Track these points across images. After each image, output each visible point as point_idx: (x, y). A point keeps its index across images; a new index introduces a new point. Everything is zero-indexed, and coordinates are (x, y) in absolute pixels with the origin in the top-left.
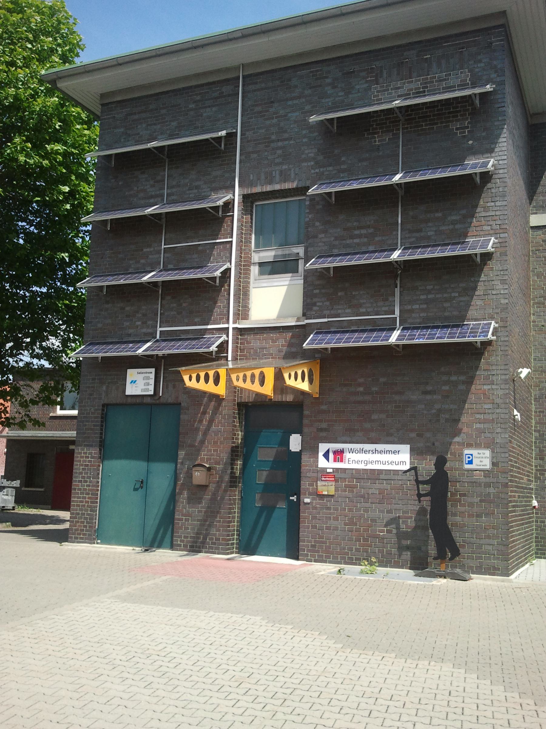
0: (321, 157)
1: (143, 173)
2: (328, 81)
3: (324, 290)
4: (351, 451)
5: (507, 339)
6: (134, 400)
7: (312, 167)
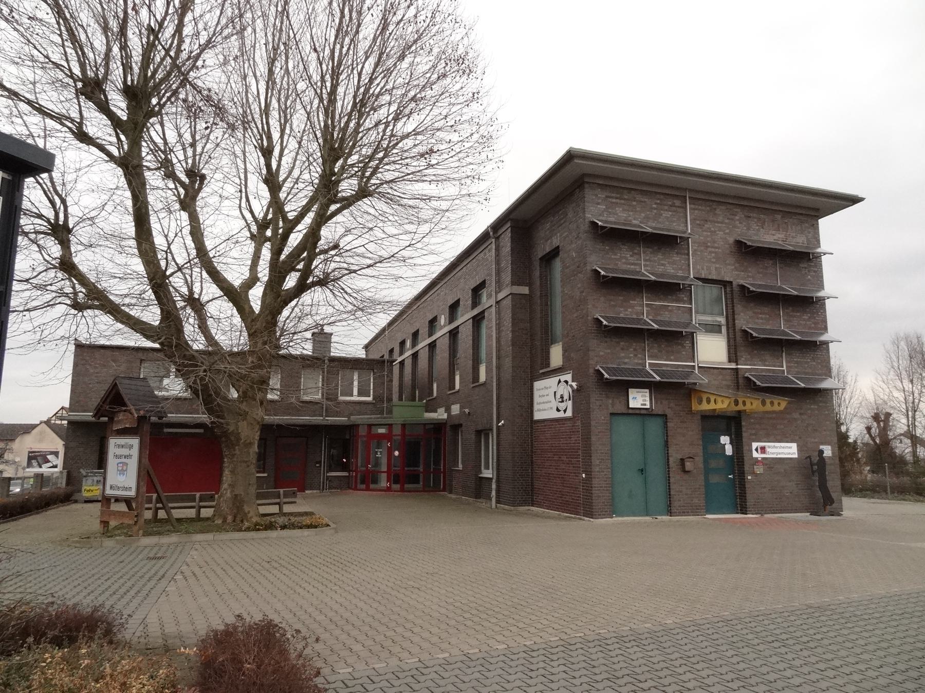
0: (737, 265)
4: (769, 447)
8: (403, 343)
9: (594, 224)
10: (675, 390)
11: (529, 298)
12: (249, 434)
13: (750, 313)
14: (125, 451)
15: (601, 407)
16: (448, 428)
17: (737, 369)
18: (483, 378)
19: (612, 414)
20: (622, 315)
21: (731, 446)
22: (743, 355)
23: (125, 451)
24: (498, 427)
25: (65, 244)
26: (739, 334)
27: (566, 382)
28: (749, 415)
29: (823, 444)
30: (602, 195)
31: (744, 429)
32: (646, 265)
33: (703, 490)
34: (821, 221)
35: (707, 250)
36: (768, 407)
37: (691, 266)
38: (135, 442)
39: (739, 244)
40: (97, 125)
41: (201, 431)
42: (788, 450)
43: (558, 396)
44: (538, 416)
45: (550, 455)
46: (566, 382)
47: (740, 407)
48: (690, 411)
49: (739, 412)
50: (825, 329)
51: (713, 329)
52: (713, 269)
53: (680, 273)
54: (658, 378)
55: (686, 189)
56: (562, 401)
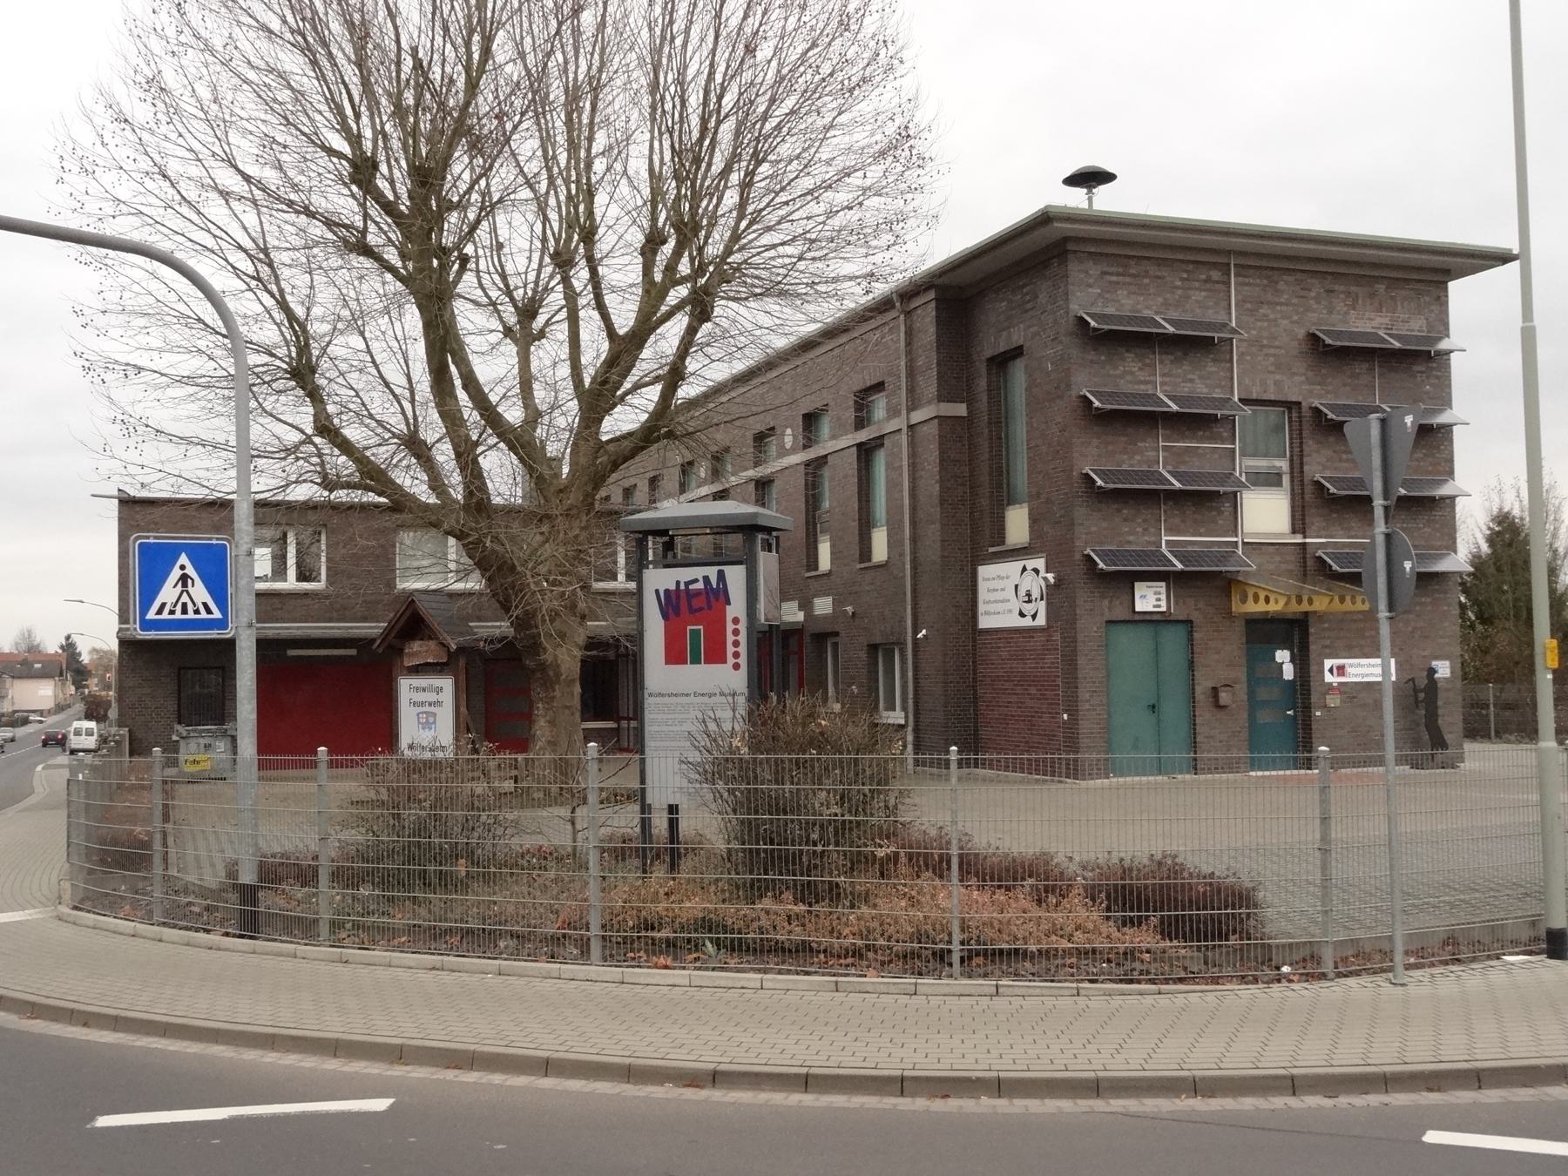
0: (1310, 374)
2: (1313, 294)
9: (1082, 322)
10: (1205, 582)
11: (968, 422)
14: (432, 697)
15: (1092, 611)
16: (807, 639)
17: (1304, 544)
18: (880, 551)
19: (1109, 622)
20: (1124, 467)
22: (1315, 522)
23: (432, 697)
24: (916, 641)
25: (315, 395)
26: (1309, 489)
27: (1036, 571)
28: (1321, 617)
29: (1437, 658)
30: (1095, 270)
31: (1311, 639)
32: (1163, 385)
33: (1245, 735)
35: (1263, 352)
36: (1348, 606)
37: (1233, 382)
38: (446, 684)
39: (1313, 338)
41: (353, 652)
43: (1022, 592)
44: (985, 622)
45: (1007, 685)
46: (1036, 571)
47: (1305, 607)
48: (1229, 615)
49: (1306, 614)
50: (1450, 473)
51: (1269, 480)
52: (1270, 382)
53: (1218, 394)
54: (1180, 566)
55: (1229, 252)
56: (1029, 601)
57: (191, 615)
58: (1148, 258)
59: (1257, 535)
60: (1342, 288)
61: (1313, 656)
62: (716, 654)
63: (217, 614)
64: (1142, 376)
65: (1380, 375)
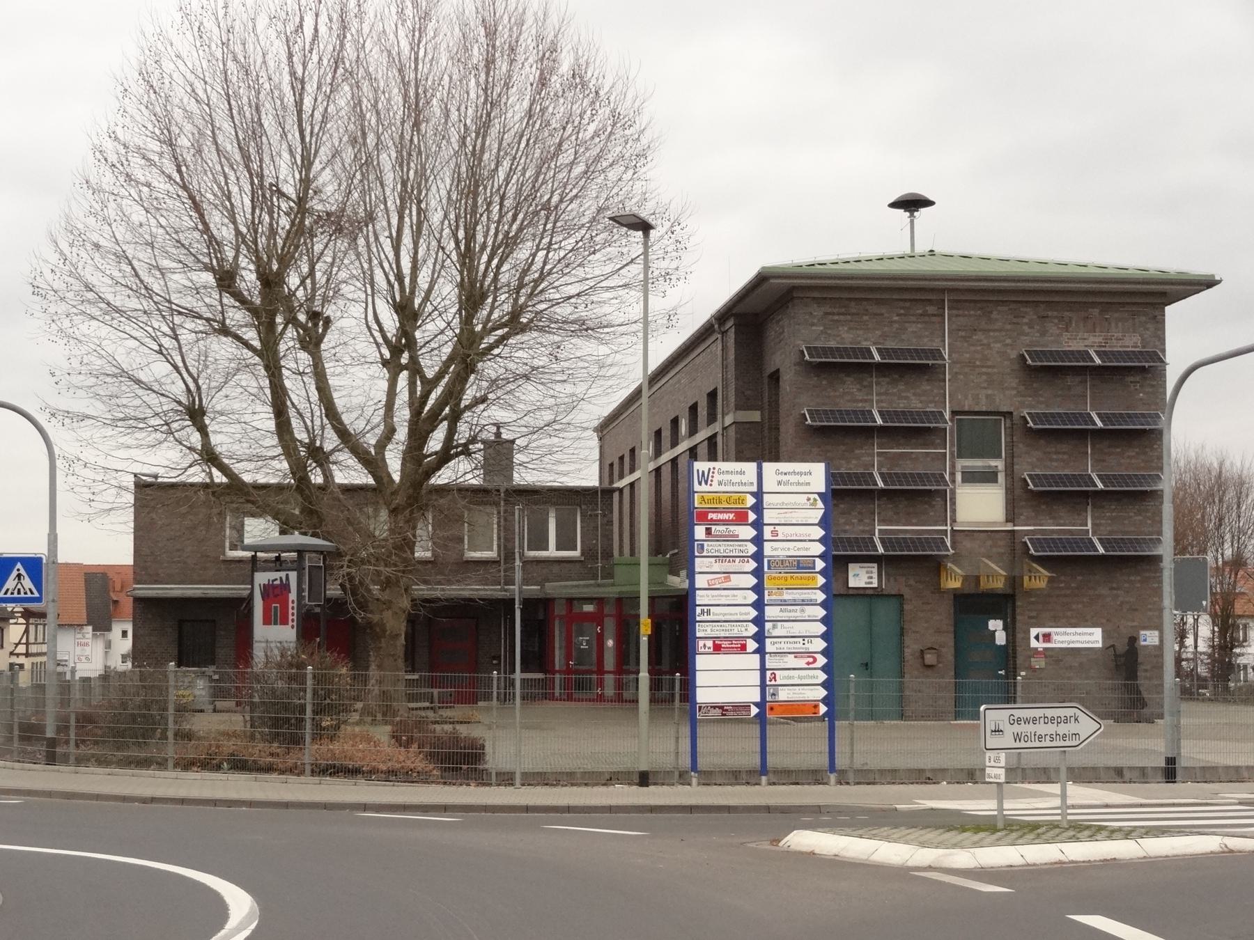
0: (1022, 388)
1: (848, 376)
2: (1025, 320)
3: (1022, 499)
4: (1057, 634)
5: (118, 165)
6: (855, 592)
7: (1015, 396)
8: (675, 422)
12: (396, 624)
13: (1038, 454)
21: (1004, 634)
25: (203, 430)
30: (818, 312)
34: (1167, 308)
35: (977, 372)
37: (945, 401)
40: (237, 316)
42: (1091, 637)
48: (937, 589)
57: (22, 595)
58: (867, 299)
59: (969, 523)
60: (1055, 313)
61: (1018, 625)
62: (284, 621)
63: (37, 595)
64: (860, 396)
65: (1093, 386)
